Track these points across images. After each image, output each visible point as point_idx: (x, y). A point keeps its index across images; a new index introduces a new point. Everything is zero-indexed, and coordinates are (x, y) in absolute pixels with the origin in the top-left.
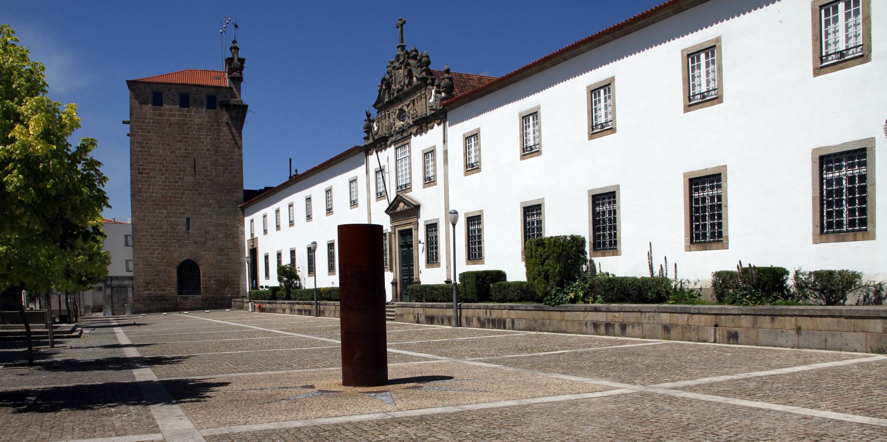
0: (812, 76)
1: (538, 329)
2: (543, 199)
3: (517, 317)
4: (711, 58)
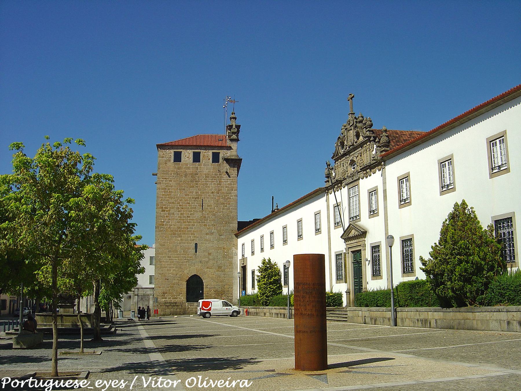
1: (456, 327)
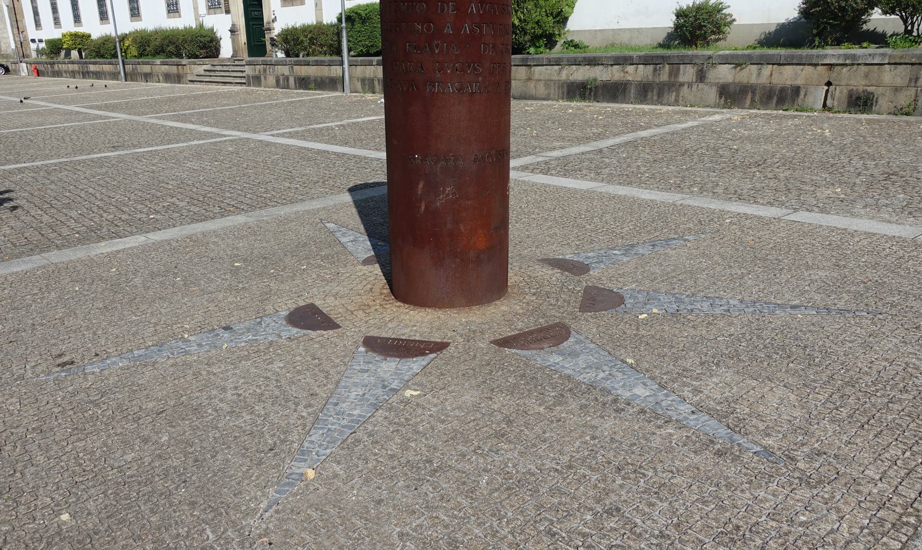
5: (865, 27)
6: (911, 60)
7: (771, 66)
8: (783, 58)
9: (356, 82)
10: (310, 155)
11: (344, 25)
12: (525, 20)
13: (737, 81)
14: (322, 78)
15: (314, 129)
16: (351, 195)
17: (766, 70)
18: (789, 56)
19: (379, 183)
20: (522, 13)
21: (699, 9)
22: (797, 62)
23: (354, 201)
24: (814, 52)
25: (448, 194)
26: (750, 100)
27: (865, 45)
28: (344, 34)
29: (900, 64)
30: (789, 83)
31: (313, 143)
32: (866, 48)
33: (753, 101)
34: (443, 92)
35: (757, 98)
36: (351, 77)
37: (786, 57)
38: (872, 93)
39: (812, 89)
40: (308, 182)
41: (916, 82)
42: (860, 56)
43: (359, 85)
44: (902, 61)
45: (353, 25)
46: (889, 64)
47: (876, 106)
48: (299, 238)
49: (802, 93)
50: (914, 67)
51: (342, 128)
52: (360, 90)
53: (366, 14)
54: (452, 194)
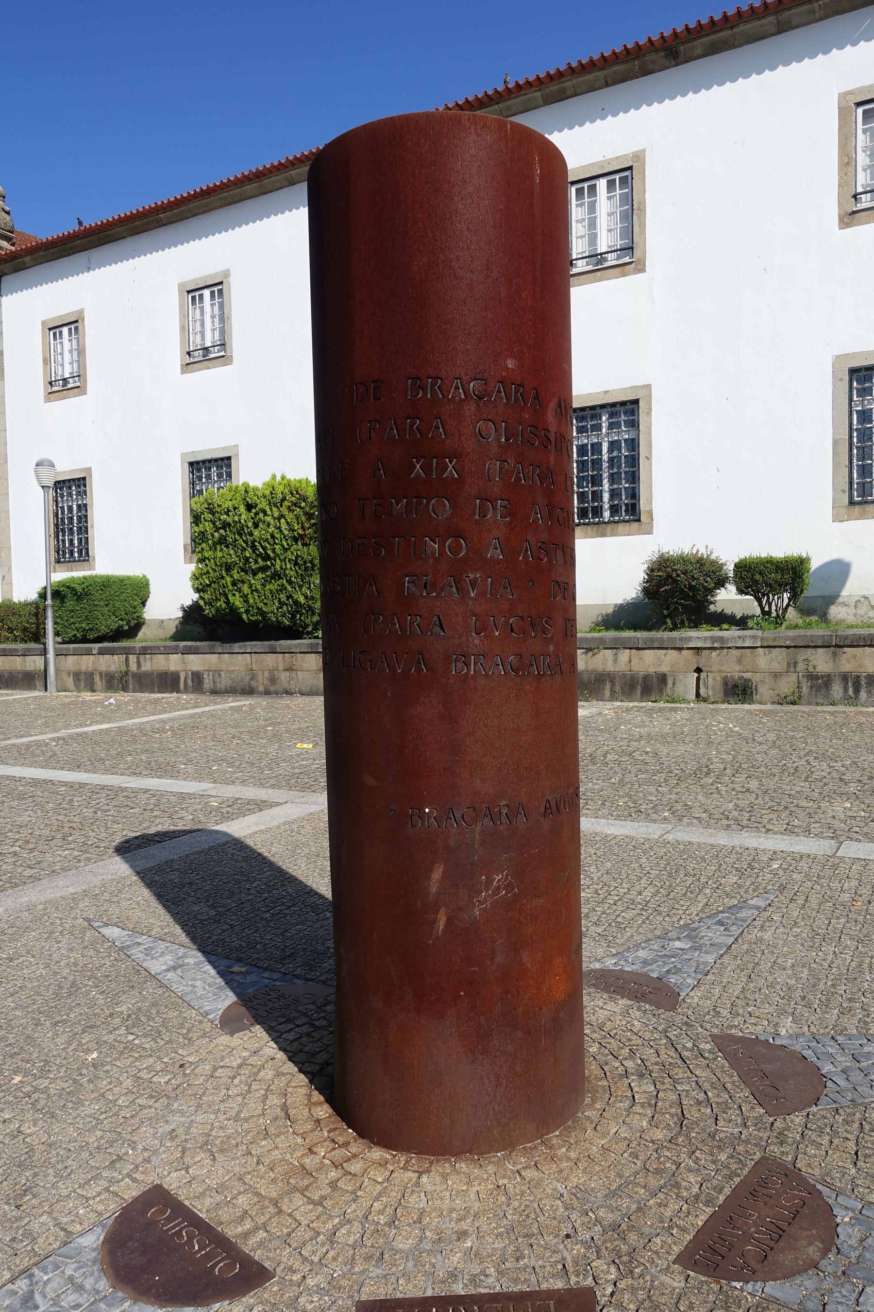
0: (837, 227)
2: (236, 446)
3: (206, 668)
4: (620, 189)
5: (712, 608)
6: (785, 643)
7: (628, 650)
8: (641, 642)
9: (65, 677)
10: (21, 788)
11: (49, 602)
12: (312, 596)
13: (589, 668)
14: (11, 673)
15: (14, 745)
16: (127, 862)
17: (624, 655)
18: (648, 639)
19: (167, 832)
20: (309, 588)
21: (651, 571)
22: (658, 646)
23: (138, 873)
24: (675, 634)
25: (498, 889)
26: (609, 691)
27: (725, 626)
28: (50, 613)
29: (774, 647)
30: (652, 670)
31: (20, 768)
32: (728, 630)
33: (613, 692)
34: (487, 675)
35: (617, 688)
36: (58, 671)
37: (645, 640)
38: (750, 680)
39: (680, 677)
40: (34, 840)
41: (795, 667)
42: (728, 639)
43: (70, 682)
44: (776, 644)
45: (63, 602)
46: (762, 647)
47: (756, 694)
48: (55, 973)
49: (670, 682)
50: (789, 650)
51: (61, 742)
52: (72, 687)
53: (83, 589)
54: (506, 888)
